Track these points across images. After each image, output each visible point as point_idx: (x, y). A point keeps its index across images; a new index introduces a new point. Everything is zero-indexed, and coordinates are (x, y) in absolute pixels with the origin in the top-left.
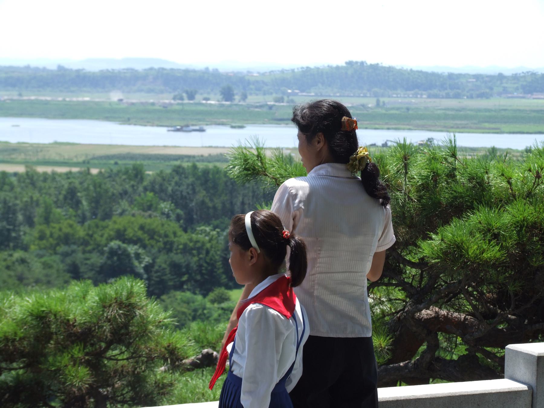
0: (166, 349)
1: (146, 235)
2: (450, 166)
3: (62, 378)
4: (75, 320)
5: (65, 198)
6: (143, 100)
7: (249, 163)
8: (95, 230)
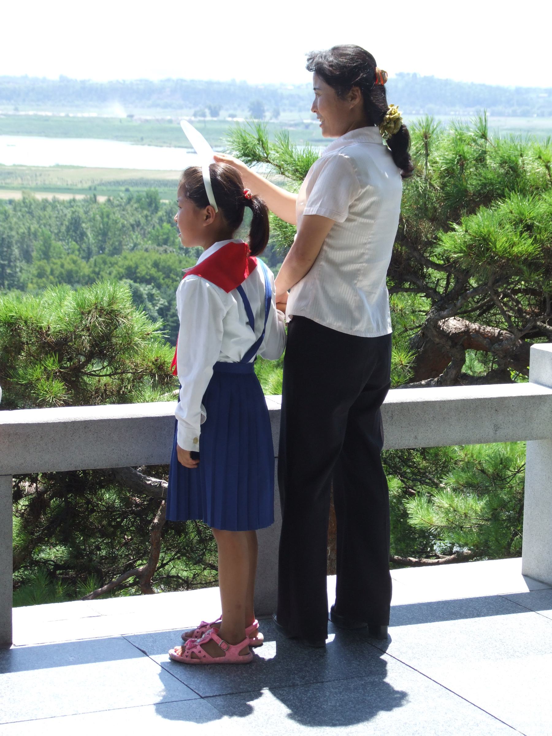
0: (153, 363)
1: (160, 273)
2: (480, 148)
3: (34, 393)
4: (49, 328)
5: (68, 229)
6: (159, 117)
7: (248, 147)
8: (102, 266)
